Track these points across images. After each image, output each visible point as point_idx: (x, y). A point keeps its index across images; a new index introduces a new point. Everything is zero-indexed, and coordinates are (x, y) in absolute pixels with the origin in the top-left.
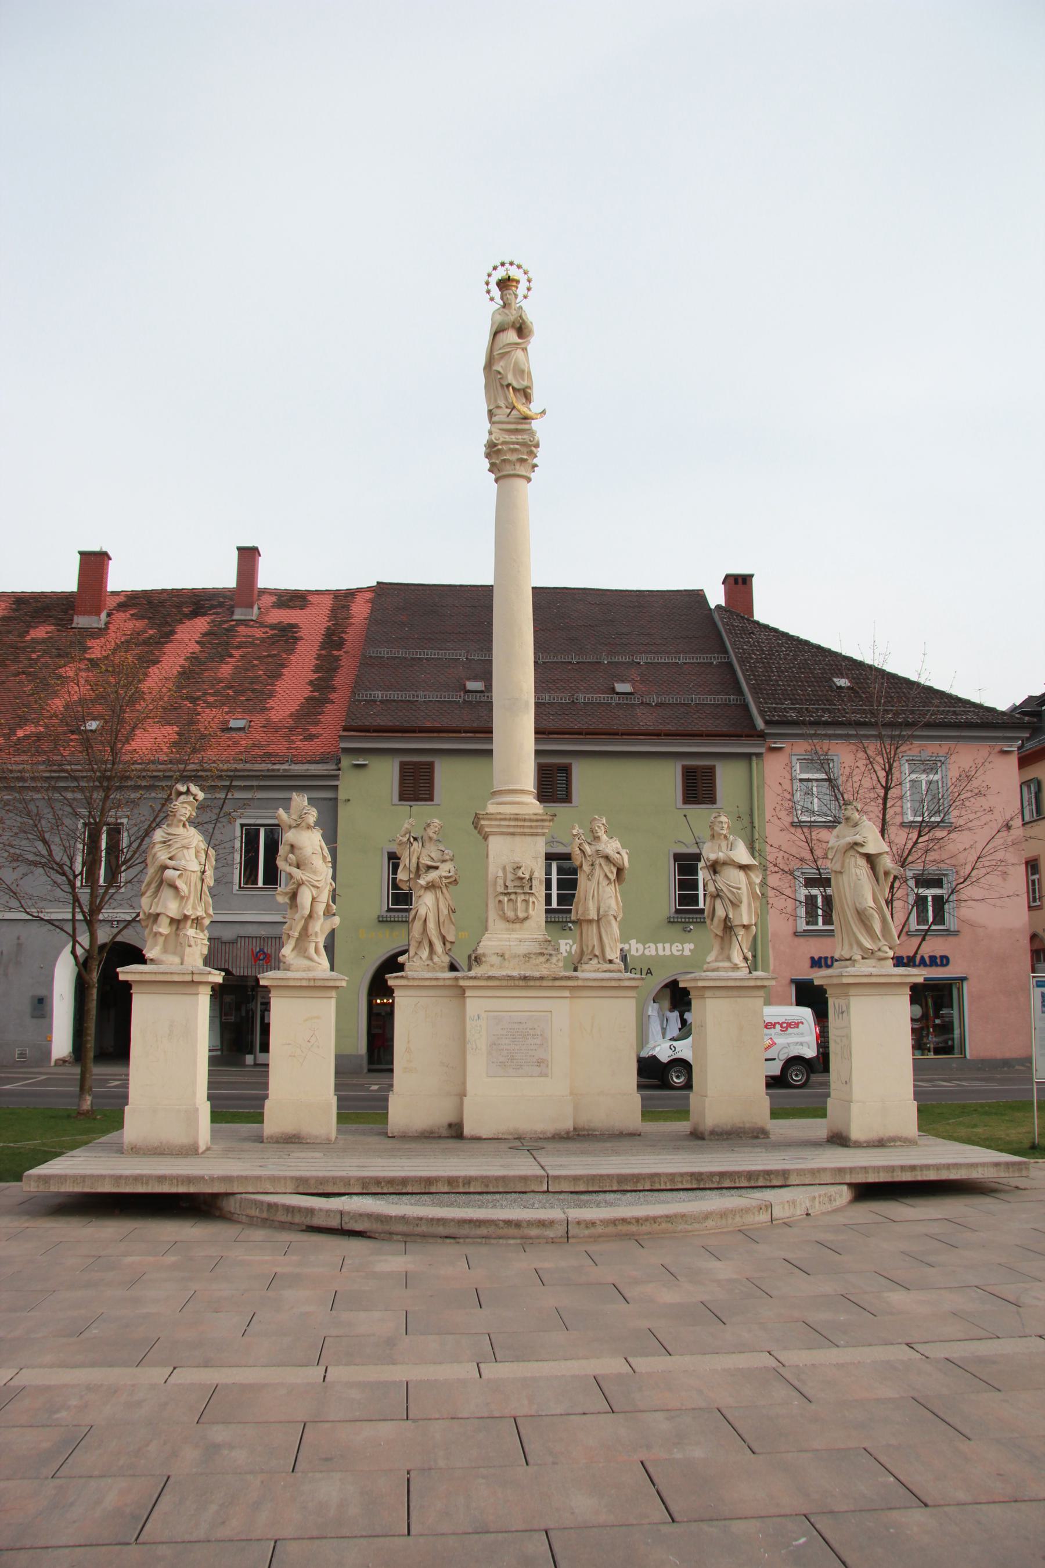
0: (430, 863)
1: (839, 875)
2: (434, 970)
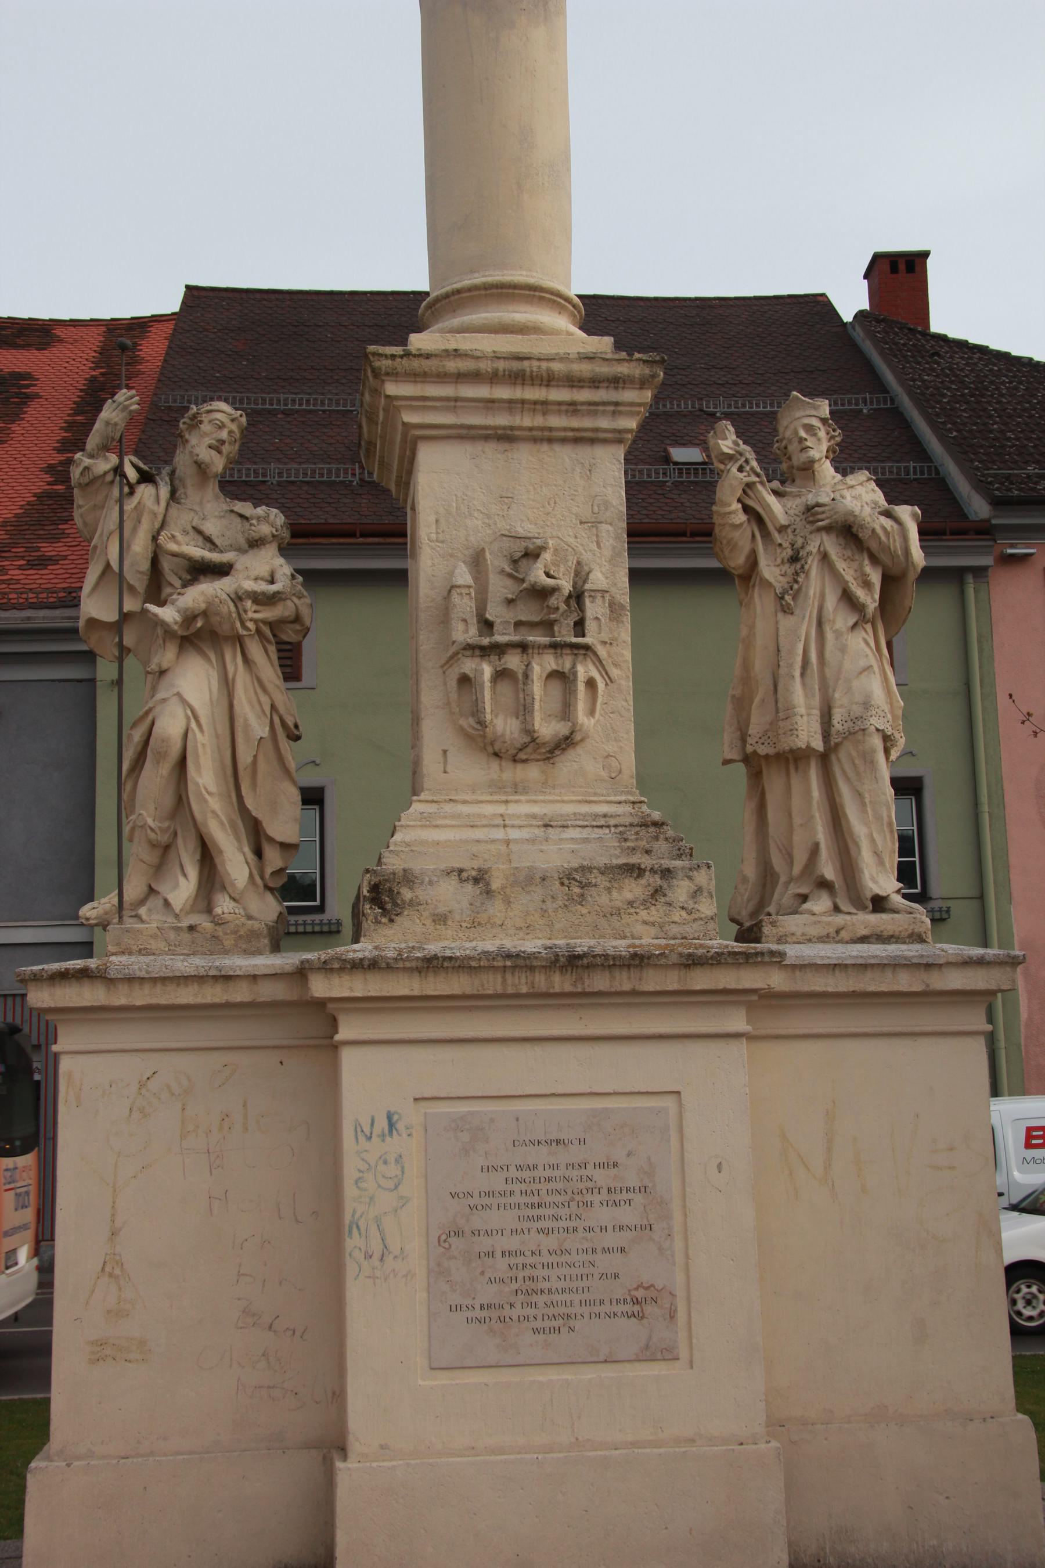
0: (198, 552)
2: (216, 945)
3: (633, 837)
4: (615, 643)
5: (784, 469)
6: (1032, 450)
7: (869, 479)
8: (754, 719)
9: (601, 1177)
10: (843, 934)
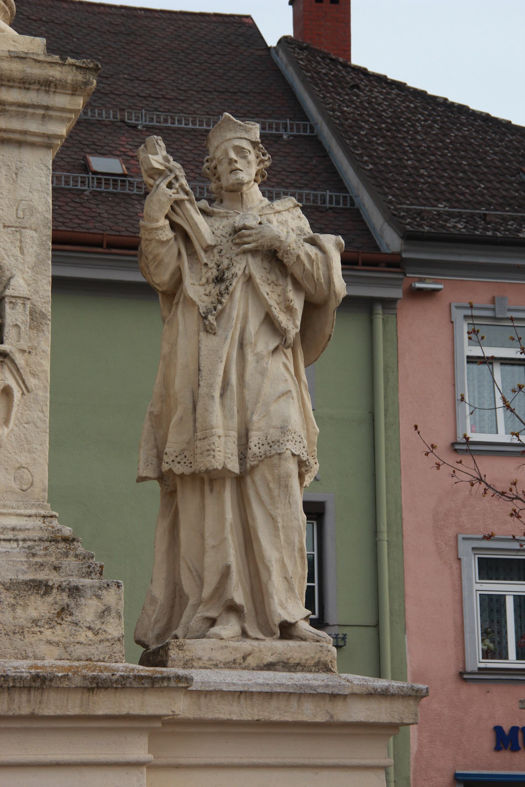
3: (42, 552)
4: (33, 353)
5: (212, 189)
6: (444, 189)
7: (296, 206)
8: (171, 438)
10: (250, 660)
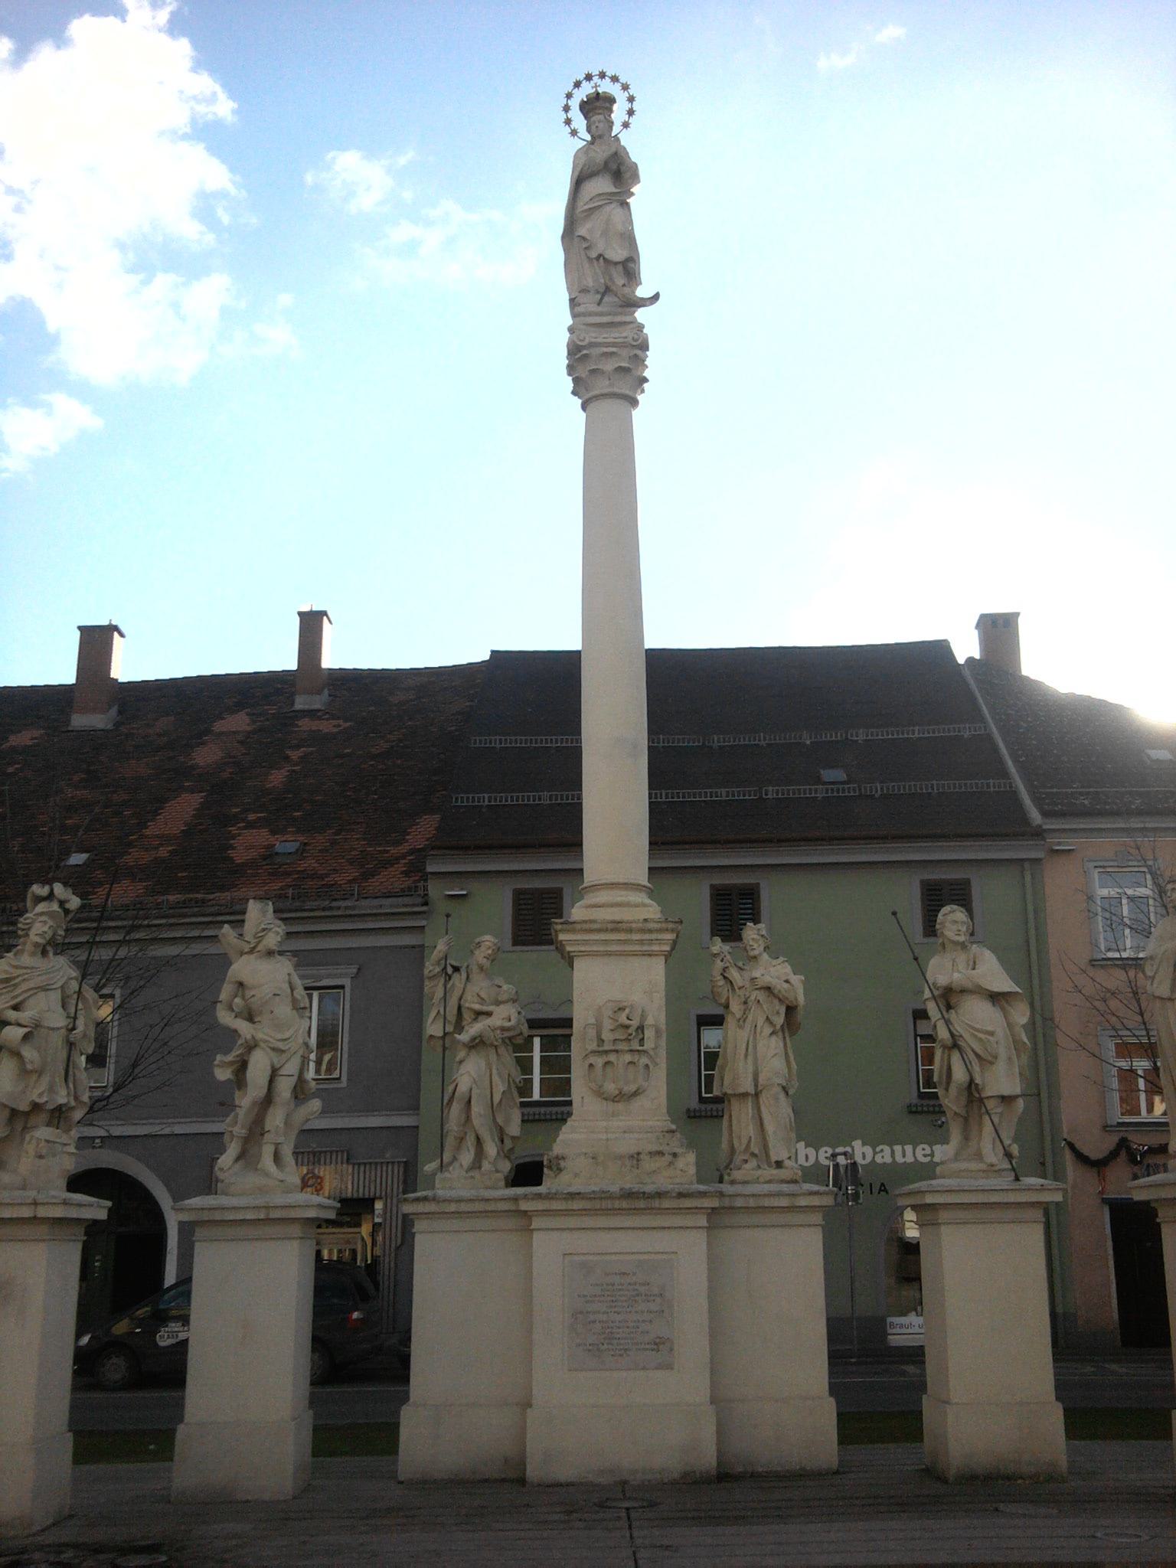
0: (477, 1007)
1: (1169, 1004)
9: (642, 1289)
